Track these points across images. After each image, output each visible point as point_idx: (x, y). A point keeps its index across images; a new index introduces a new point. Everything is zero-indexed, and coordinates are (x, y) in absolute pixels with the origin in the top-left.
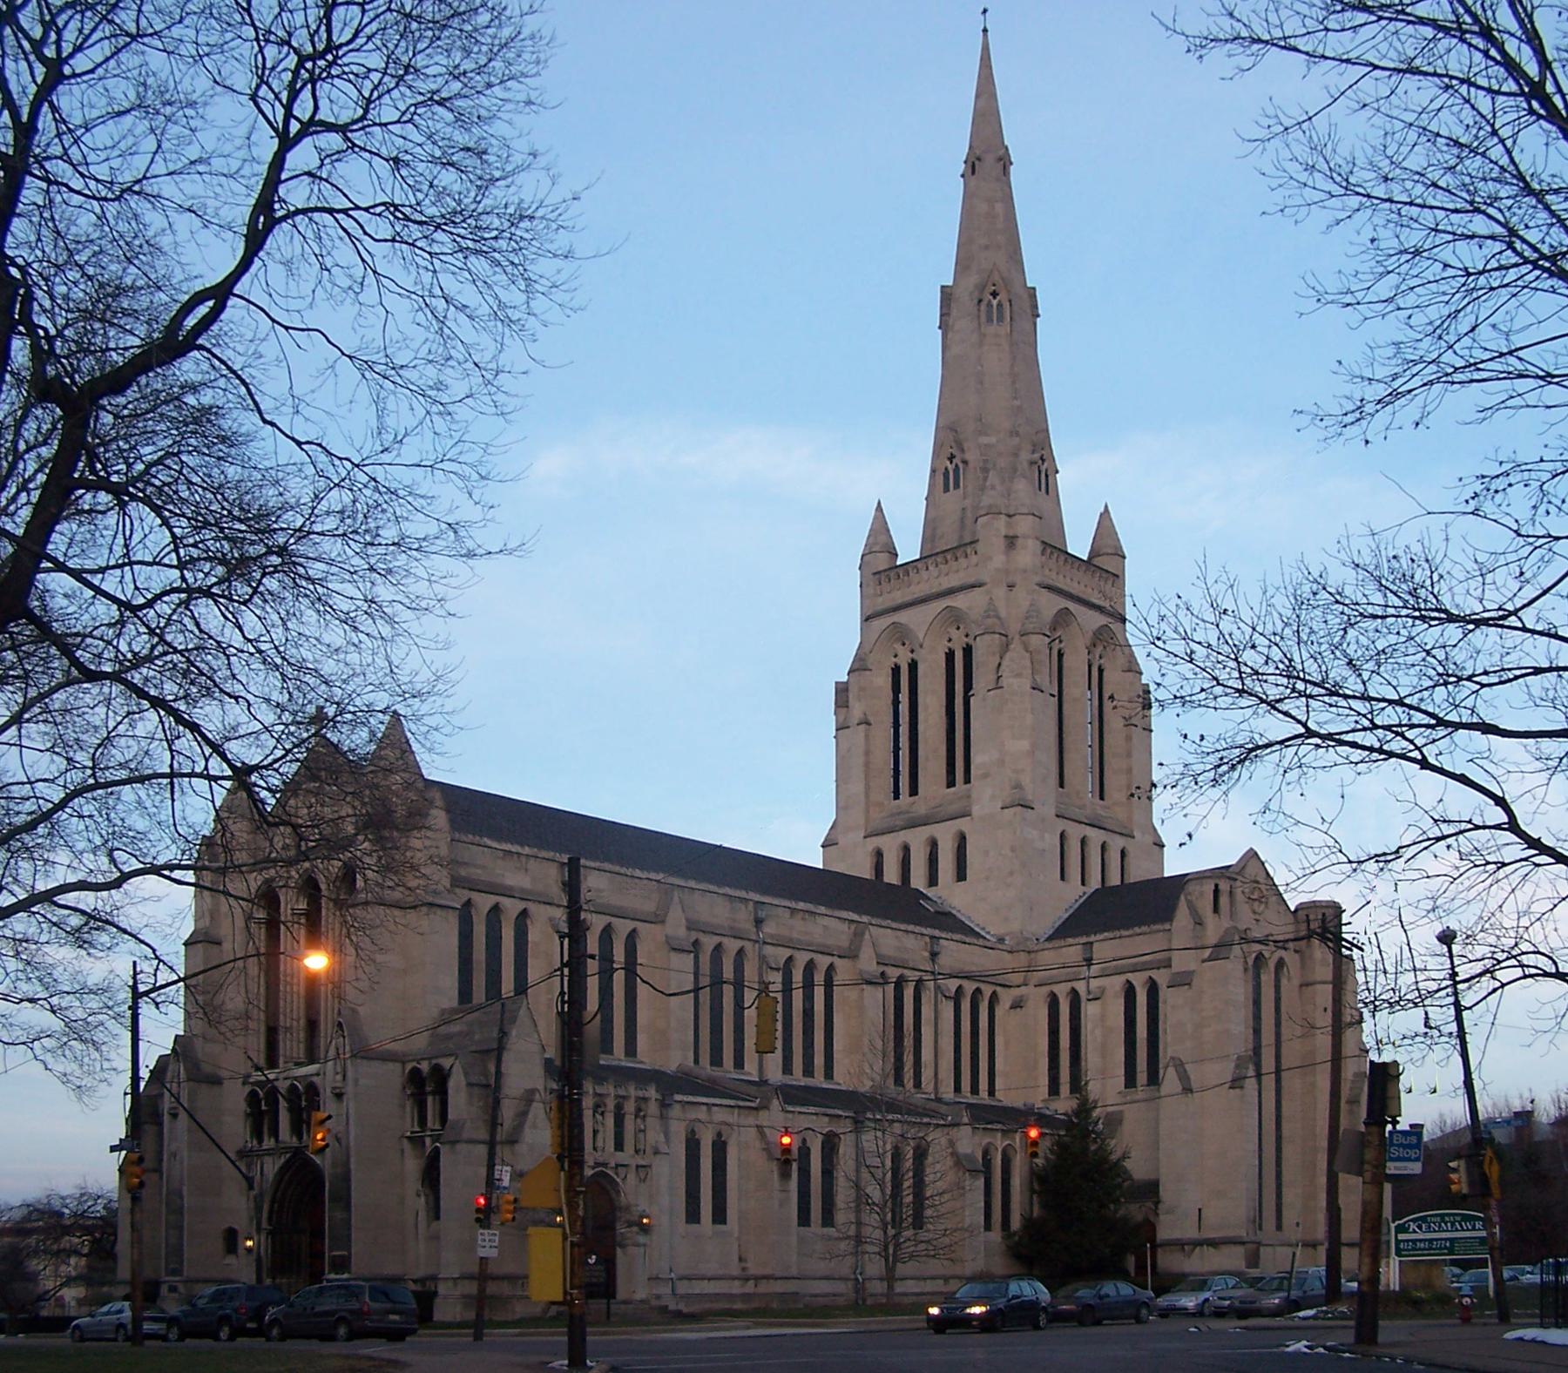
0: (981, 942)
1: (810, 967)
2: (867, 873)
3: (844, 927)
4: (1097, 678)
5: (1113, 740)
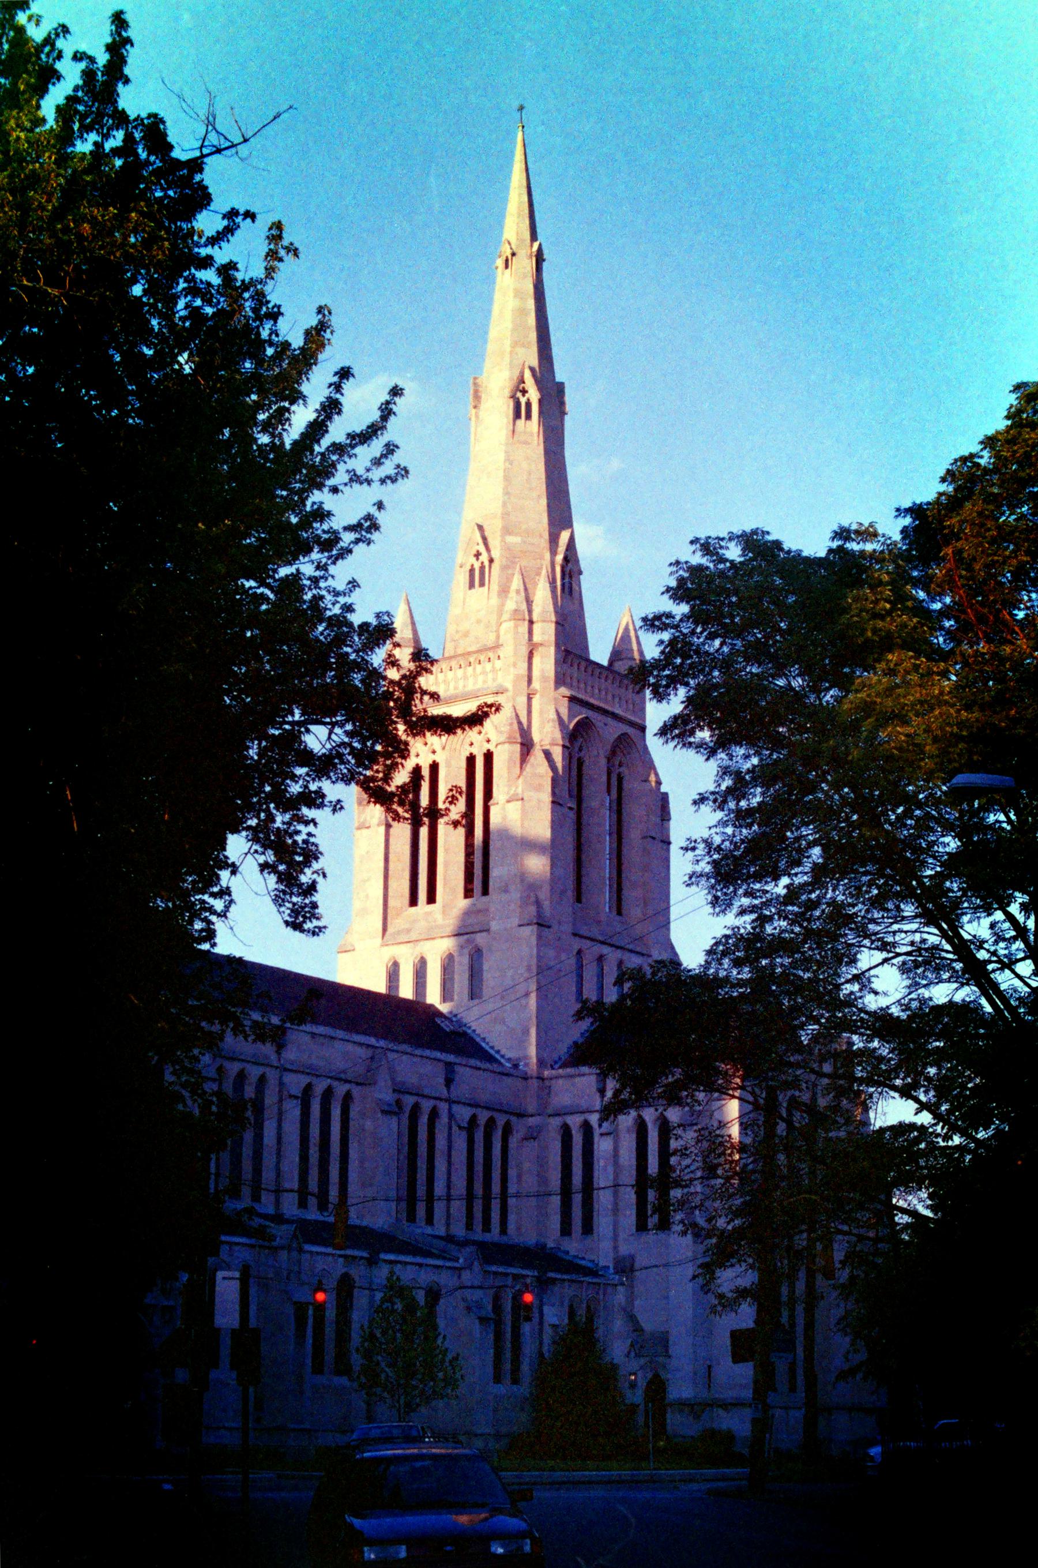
0: (495, 1067)
1: (328, 1093)
2: (378, 985)
3: (361, 1052)
4: (617, 785)
5: (633, 854)
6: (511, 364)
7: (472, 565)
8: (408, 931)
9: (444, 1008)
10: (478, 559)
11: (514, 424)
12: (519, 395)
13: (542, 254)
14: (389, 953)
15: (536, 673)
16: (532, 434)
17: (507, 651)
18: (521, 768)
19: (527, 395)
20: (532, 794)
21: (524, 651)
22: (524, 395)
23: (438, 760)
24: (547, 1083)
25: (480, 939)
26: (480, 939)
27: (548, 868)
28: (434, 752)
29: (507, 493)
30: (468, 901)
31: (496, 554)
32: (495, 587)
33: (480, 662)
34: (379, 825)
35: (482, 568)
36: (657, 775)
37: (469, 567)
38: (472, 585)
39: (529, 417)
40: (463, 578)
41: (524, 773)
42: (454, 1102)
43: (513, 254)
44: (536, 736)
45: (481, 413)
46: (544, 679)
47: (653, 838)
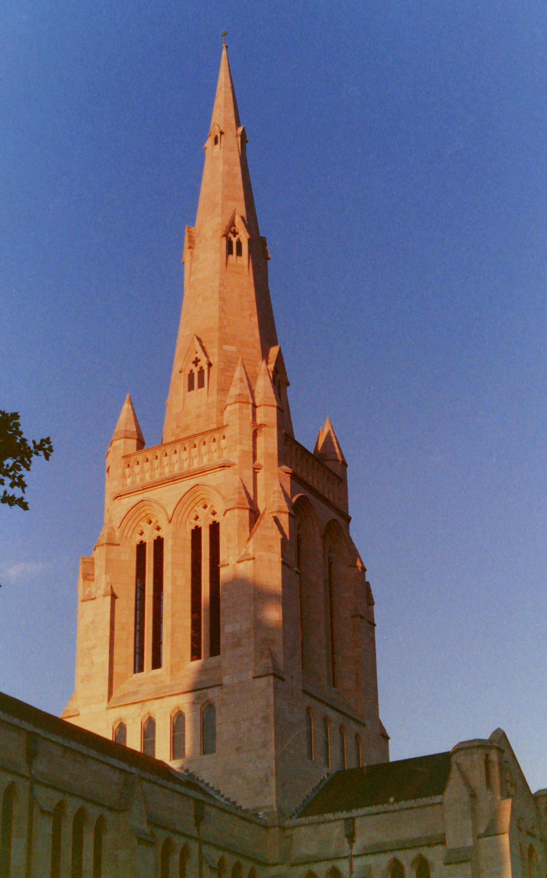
3: (116, 777)
6: (223, 211)
7: (191, 371)
8: (136, 693)
9: (175, 765)
10: (196, 365)
11: (227, 259)
12: (231, 235)
13: (246, 137)
14: (115, 714)
15: (259, 451)
16: (243, 266)
17: (232, 431)
18: (250, 531)
19: (237, 236)
20: (264, 554)
21: (249, 431)
22: (235, 236)
24: (288, 832)
25: (213, 694)
26: (213, 694)
27: (281, 619)
28: (158, 529)
29: (222, 310)
30: (196, 664)
31: (214, 360)
32: (214, 387)
34: (105, 595)
35: (201, 372)
36: (362, 563)
37: (188, 372)
38: (191, 388)
39: (239, 253)
40: (183, 381)
41: (255, 535)
42: (205, 843)
43: (222, 133)
44: (261, 506)
45: (196, 252)
46: (268, 456)
47: (362, 618)
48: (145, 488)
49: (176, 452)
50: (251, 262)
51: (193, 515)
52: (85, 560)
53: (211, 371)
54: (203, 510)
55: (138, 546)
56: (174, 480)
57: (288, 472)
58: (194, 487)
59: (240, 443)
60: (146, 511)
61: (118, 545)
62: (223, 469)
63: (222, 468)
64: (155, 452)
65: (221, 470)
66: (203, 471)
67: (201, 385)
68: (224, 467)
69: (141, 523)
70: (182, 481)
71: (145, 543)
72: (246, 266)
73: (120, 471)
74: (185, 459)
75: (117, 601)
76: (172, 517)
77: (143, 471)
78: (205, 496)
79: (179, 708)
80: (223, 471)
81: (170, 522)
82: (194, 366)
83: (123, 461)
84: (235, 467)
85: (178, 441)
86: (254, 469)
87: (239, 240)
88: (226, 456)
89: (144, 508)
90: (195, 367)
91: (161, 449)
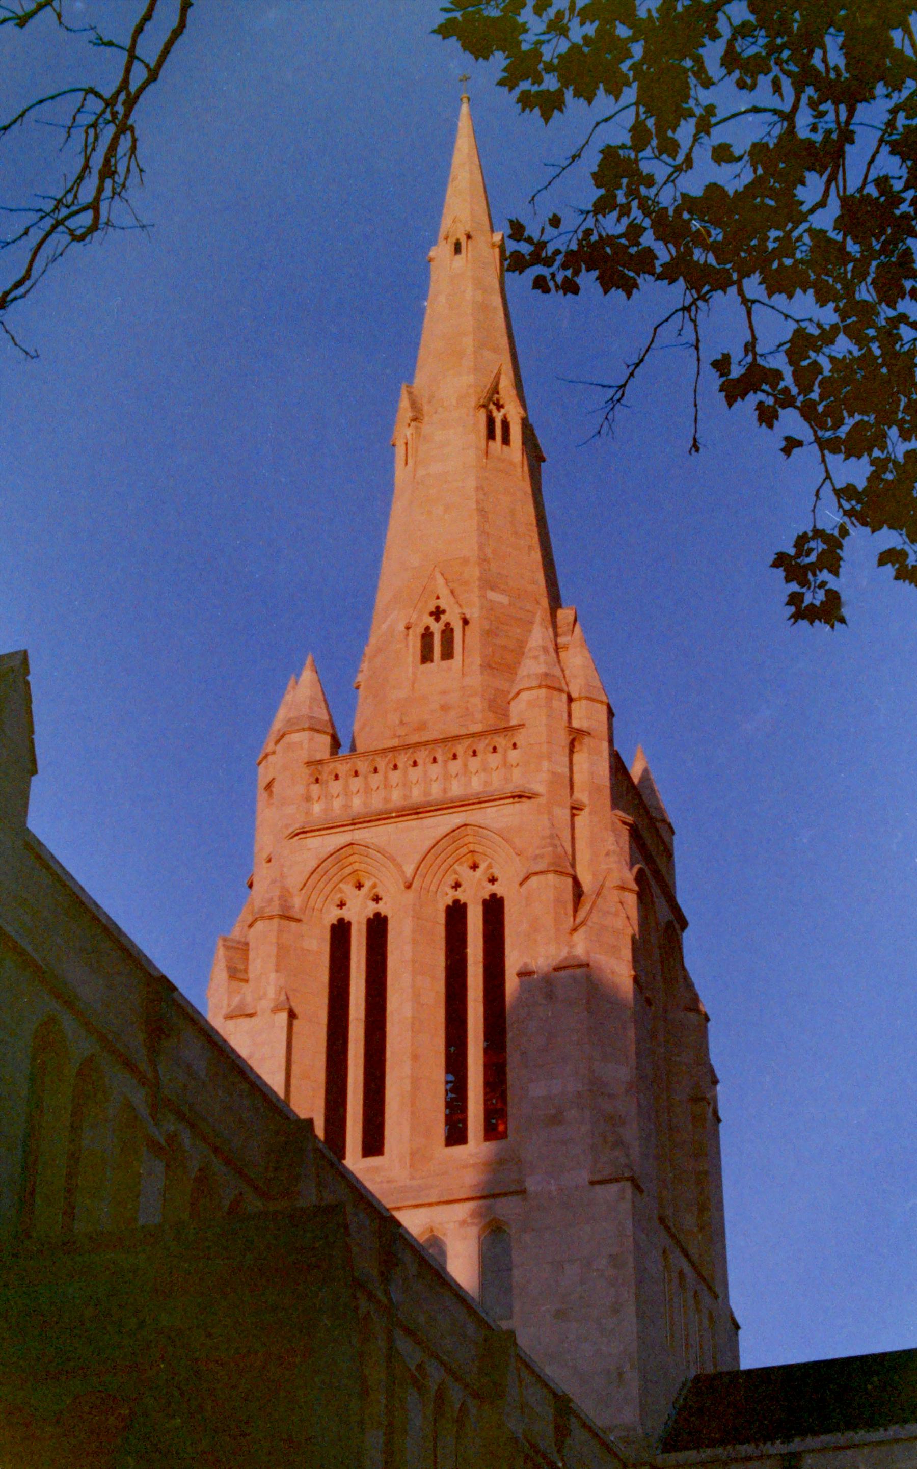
7: (427, 628)
10: (437, 619)
12: (492, 407)
16: (511, 463)
19: (503, 411)
21: (563, 738)
23: (463, 899)
26: (507, 1208)
29: (483, 533)
33: (475, 753)
34: (275, 1010)
38: (426, 657)
39: (506, 441)
45: (426, 429)
48: (355, 822)
49: (415, 764)
50: (525, 456)
51: (451, 880)
52: (226, 943)
53: (468, 632)
54: (356, 891)
55: (333, 928)
56: (417, 813)
57: (627, 821)
58: (342, 848)
59: (549, 758)
60: (353, 865)
61: (299, 921)
62: (519, 802)
63: (516, 800)
64: (373, 760)
65: (513, 803)
66: (479, 801)
67: (448, 654)
68: (520, 797)
69: (341, 885)
70: (473, 809)
71: (349, 923)
72: (519, 465)
73: (300, 789)
74: (356, 790)
75: (296, 1022)
76: (413, 878)
77: (347, 793)
78: (478, 848)
79: (432, 1231)
80: (517, 805)
81: (409, 887)
82: (433, 621)
83: (306, 771)
84: (543, 800)
85: (406, 747)
86: (573, 808)
87: (505, 416)
88: (517, 780)
89: (351, 859)
90: (435, 623)
91: (386, 757)
